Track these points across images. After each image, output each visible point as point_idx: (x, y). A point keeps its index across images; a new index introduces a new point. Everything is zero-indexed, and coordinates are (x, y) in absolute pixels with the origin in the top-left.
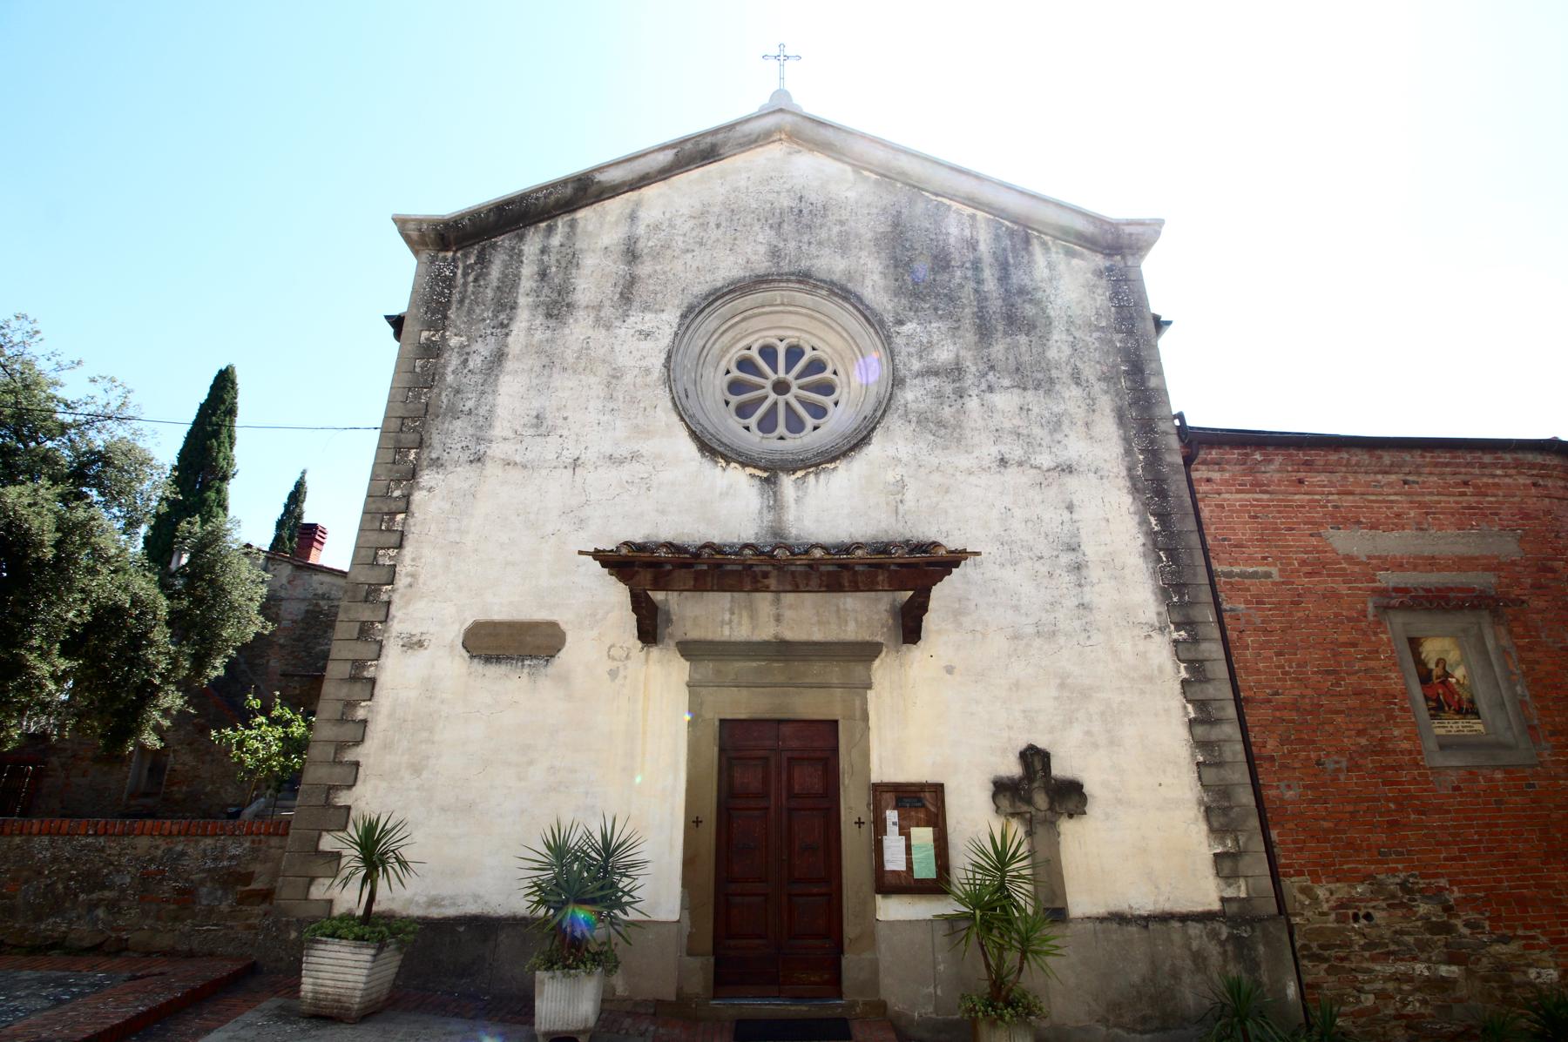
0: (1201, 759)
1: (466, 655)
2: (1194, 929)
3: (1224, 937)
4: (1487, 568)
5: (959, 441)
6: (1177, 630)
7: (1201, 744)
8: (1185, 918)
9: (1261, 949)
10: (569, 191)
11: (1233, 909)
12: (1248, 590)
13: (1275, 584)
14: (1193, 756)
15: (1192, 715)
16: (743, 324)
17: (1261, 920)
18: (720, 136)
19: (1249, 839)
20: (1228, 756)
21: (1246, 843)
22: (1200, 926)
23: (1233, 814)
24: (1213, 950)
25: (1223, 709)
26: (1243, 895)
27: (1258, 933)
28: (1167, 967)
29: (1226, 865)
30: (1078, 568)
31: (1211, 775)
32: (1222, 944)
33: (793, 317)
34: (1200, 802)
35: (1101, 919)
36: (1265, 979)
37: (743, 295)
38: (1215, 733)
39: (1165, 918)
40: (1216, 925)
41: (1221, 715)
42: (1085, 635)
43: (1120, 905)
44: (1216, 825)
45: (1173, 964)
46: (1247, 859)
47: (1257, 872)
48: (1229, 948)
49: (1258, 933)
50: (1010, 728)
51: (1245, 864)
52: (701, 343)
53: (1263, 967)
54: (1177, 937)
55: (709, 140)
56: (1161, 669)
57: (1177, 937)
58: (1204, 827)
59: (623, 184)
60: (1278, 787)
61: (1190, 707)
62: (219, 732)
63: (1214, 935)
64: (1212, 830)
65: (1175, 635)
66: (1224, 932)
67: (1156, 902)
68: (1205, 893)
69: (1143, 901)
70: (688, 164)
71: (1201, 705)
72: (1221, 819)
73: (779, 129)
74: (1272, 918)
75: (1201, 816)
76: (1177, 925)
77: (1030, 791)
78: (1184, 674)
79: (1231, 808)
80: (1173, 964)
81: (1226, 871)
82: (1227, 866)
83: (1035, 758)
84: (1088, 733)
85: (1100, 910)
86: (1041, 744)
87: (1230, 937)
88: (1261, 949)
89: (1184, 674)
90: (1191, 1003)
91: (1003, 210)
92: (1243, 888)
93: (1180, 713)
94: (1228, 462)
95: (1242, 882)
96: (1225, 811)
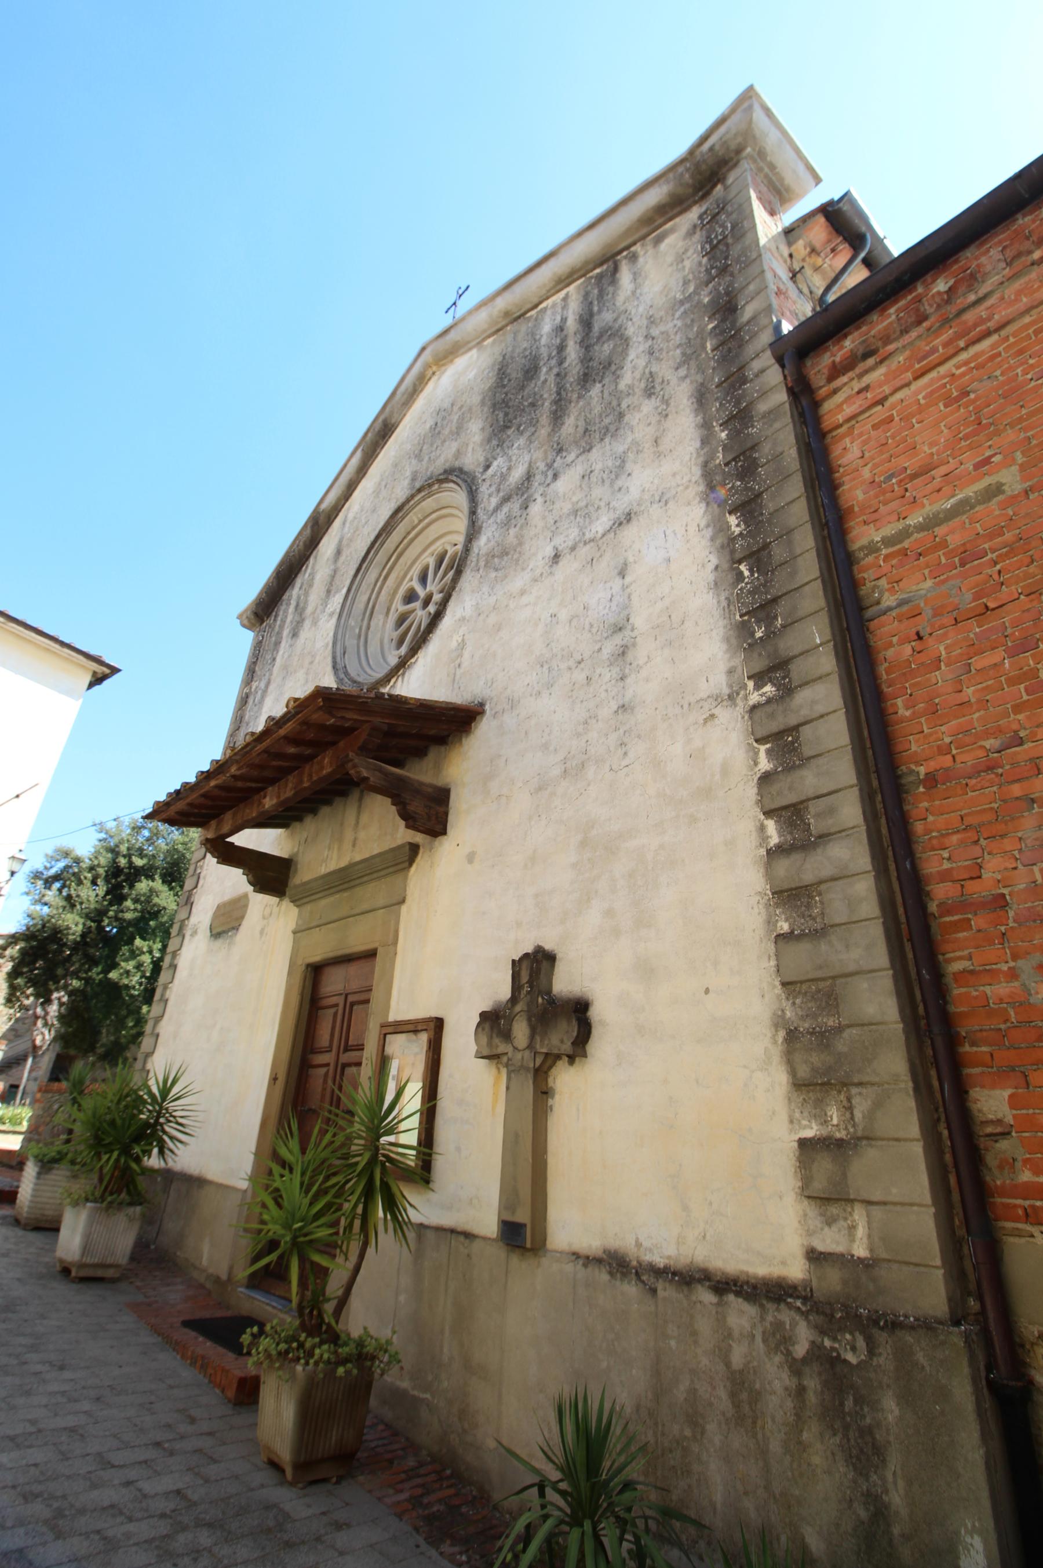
0: (784, 927)
1: (209, 934)
2: (741, 1315)
3: (800, 1350)
4: (601, 264)
5: (517, 564)
6: (758, 687)
7: (790, 896)
8: (725, 1286)
9: (891, 1409)
10: (308, 531)
11: (833, 1280)
12: (944, 544)
13: (1013, 499)
14: (770, 923)
15: (774, 840)
16: (401, 561)
17: (894, 1325)
18: (388, 410)
19: (878, 1105)
20: (838, 912)
21: (870, 1116)
22: (751, 1310)
23: (841, 1045)
24: (776, 1378)
25: (831, 811)
26: (860, 1251)
27: (885, 1359)
28: (680, 1393)
29: (827, 1167)
30: (623, 652)
31: (803, 959)
32: (796, 1367)
33: (432, 527)
34: (779, 1021)
35: (588, 1260)
36: (896, 1499)
37: (389, 534)
38: (812, 867)
39: (687, 1277)
40: (786, 1316)
41: (828, 824)
42: (620, 752)
43: (624, 1241)
44: (803, 1071)
45: (693, 1391)
46: (870, 1156)
47: (895, 1193)
48: (812, 1383)
49: (885, 1359)
50: (519, 924)
51: (866, 1169)
52: (365, 598)
53: (894, 1461)
54: (704, 1326)
55: (381, 420)
56: (725, 770)
57: (704, 1326)
58: (781, 1077)
59: (339, 500)
60: (1013, 975)
61: (771, 825)
62: (32, 994)
63: (779, 1340)
64: (799, 1085)
65: (755, 698)
66: (804, 1338)
67: (680, 1240)
68: (772, 1233)
69: (662, 1240)
70: (375, 450)
71: (790, 813)
72: (815, 1059)
73: (428, 366)
74: (926, 1325)
75: (776, 1052)
76: (706, 1296)
77: (511, 1020)
78: (765, 764)
79: (840, 1029)
80: (693, 1391)
81: (819, 1185)
82: (824, 1165)
83: (535, 966)
84: (609, 913)
85: (591, 1243)
86: (548, 947)
87: (816, 1353)
88: (891, 1409)
89: (765, 764)
90: (718, 1498)
91: (586, 263)
92: (861, 1232)
93: (754, 839)
94: (887, 340)
95: (859, 1215)
96: (823, 1038)
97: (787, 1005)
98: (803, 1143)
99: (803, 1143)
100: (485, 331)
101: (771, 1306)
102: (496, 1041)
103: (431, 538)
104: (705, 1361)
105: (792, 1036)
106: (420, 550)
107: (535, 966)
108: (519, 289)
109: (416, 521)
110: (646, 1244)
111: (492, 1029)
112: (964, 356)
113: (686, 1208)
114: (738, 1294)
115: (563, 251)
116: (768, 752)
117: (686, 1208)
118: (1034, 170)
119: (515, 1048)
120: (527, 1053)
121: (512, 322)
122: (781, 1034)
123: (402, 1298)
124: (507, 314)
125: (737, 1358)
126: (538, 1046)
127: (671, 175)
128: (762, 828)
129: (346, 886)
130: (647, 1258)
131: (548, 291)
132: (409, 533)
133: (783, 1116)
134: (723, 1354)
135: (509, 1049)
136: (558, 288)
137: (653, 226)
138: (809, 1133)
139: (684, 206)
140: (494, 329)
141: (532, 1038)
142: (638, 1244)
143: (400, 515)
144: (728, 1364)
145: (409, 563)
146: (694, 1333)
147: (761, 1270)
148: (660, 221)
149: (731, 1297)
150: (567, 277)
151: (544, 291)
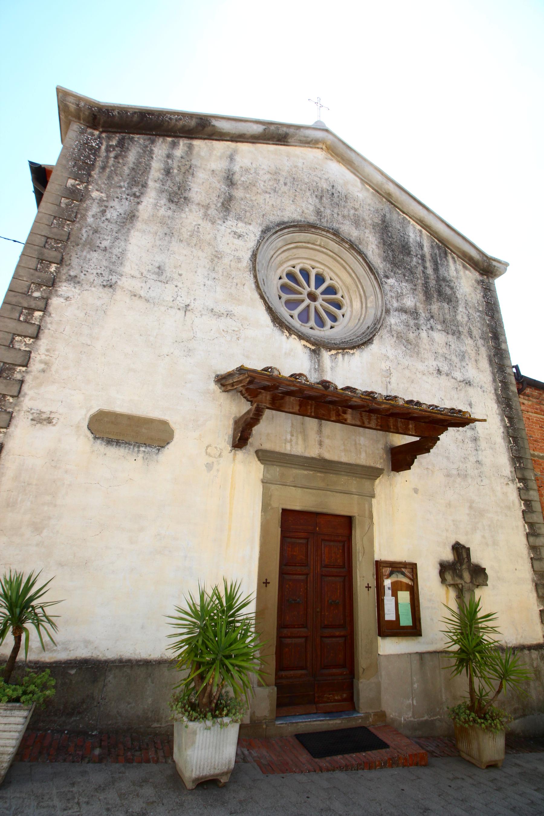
0: (532, 556)
1: (91, 436)
2: (535, 654)
8: (530, 648)
22: (536, 652)
37: (300, 231)
54: (527, 660)
57: (527, 660)
67: (517, 639)
70: (269, 140)
76: (526, 652)
84: (483, 537)
89: (523, 507)
91: (436, 233)
97: (534, 576)
98: (540, 611)
99: (540, 611)
100: (371, 181)
101: (540, 650)
102: (456, 579)
103: (316, 258)
104: (528, 668)
105: (536, 585)
106: (306, 257)
107: (460, 550)
108: (414, 204)
109: (318, 243)
110: (508, 642)
111: (453, 573)
112: (538, 416)
113: (517, 630)
114: (533, 649)
115: (432, 214)
116: (524, 504)
117: (517, 630)
118: (116, 113)
119: (465, 582)
120: (471, 584)
121: (386, 199)
122: (534, 584)
123: (415, 686)
124: (389, 194)
125: (535, 665)
126: (474, 582)
127: (485, 258)
128: (524, 526)
129: (324, 470)
130: (509, 645)
131: (413, 216)
132: (308, 243)
133: (536, 605)
134: (532, 665)
135: (463, 582)
136: (418, 222)
137: (463, 257)
138: (541, 608)
139: (476, 268)
140: (377, 189)
141: (472, 579)
142: (506, 642)
143: (313, 230)
144: (533, 667)
145: (296, 256)
146: (525, 662)
147: (535, 642)
148: (466, 260)
149: (532, 651)
150: (425, 225)
151: (412, 214)
